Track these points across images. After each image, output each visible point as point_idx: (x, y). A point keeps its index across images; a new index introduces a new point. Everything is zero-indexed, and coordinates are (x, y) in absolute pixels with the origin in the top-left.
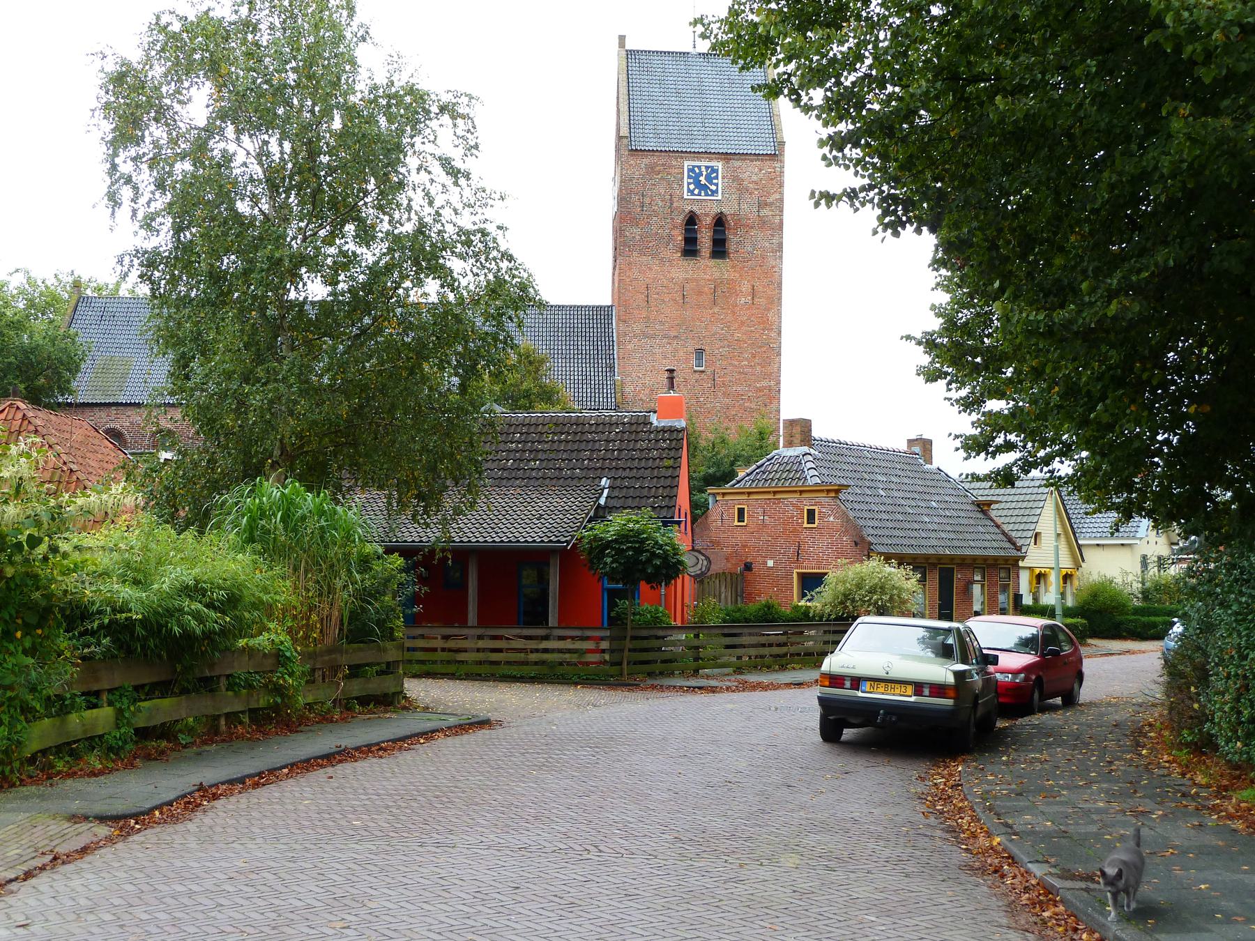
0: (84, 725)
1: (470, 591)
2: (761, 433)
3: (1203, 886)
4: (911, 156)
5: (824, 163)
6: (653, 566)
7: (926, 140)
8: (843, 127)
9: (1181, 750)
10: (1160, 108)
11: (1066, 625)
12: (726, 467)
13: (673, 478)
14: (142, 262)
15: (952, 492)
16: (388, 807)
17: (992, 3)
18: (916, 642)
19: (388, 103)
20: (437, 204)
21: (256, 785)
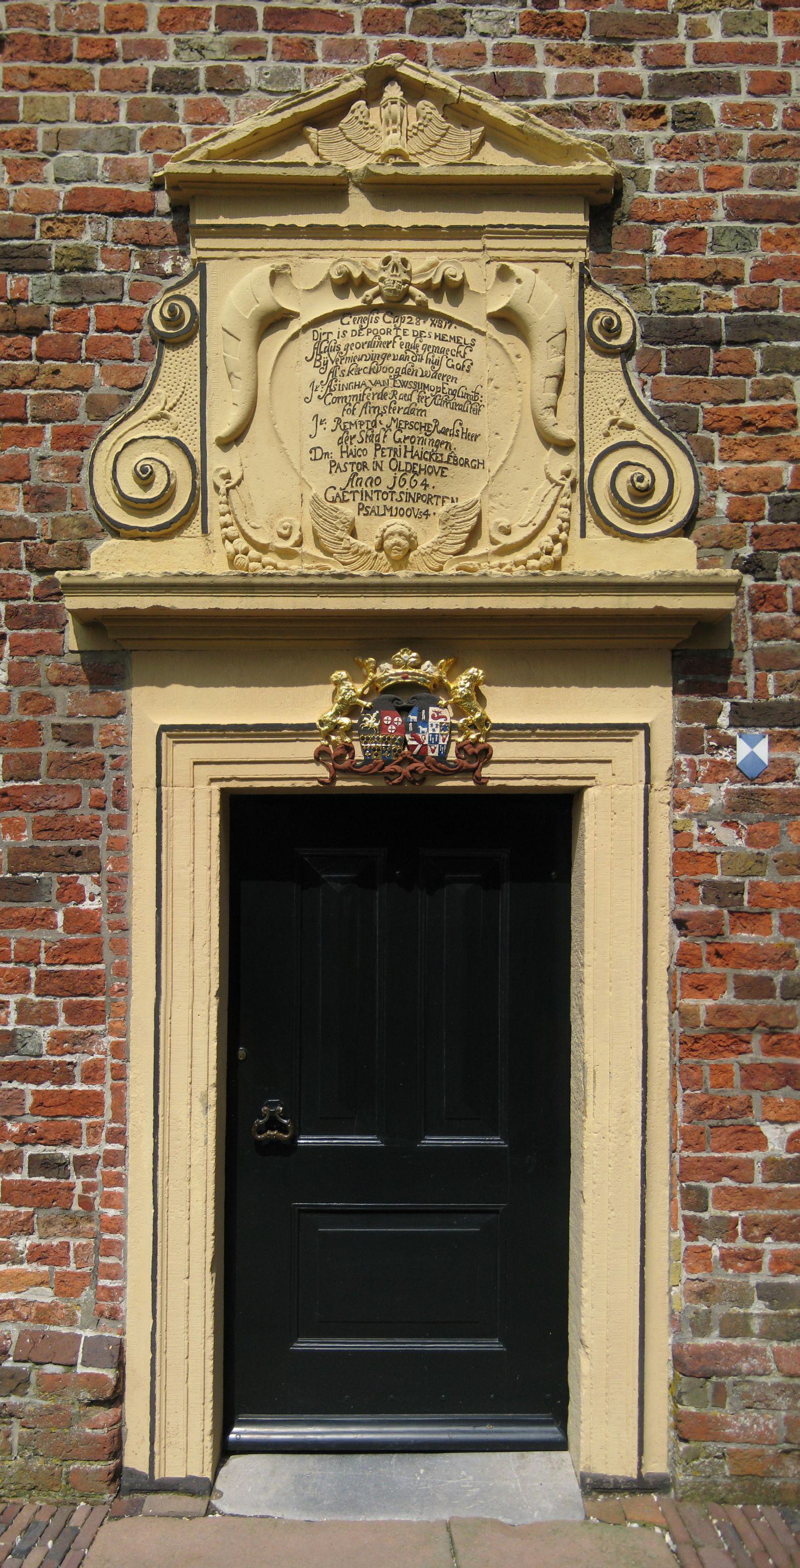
0: (669, 803)
1: (200, 606)
2: (477, 436)
3: (719, 1533)
4: (685, 1365)
5: (356, 274)
6: (711, 1382)
7: (755, 1426)
8: (445, 416)
9: (460, 749)
10: (421, 99)
11: (652, 406)
12: (140, 382)
13: (702, 1295)
14: (744, 1486)
15: (769, 548)
16: (43, 920)
17: (2, 1127)
18: (485, 318)
19: (382, 721)
20: (171, 414)
21: (671, 1217)
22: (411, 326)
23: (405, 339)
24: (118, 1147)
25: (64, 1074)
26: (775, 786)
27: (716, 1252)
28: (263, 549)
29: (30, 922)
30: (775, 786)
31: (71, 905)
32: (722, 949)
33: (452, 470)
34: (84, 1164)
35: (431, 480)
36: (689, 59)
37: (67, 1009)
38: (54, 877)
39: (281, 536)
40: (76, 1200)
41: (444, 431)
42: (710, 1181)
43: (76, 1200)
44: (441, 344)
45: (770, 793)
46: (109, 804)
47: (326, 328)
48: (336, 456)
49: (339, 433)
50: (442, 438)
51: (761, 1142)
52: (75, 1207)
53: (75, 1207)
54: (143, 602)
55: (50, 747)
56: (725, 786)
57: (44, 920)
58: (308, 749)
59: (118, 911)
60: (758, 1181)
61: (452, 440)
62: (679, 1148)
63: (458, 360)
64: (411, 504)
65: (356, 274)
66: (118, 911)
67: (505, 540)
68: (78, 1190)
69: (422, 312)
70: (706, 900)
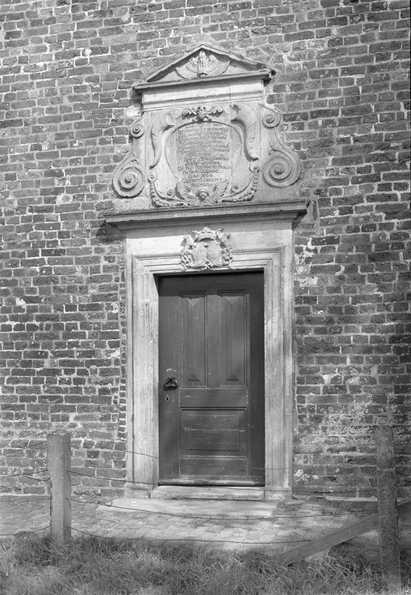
5: (190, 113)
22: (205, 126)
23: (205, 132)
24: (124, 385)
25: (109, 362)
26: (327, 264)
27: (53, 310)
28: (164, 199)
29: (98, 317)
30: (327, 264)
31: (109, 311)
32: (310, 319)
33: (221, 170)
34: (114, 390)
35: (214, 174)
36: (297, 28)
37: (110, 343)
38: (105, 303)
39: (168, 194)
40: (112, 402)
41: (217, 159)
42: (306, 394)
43: (112, 402)
44: (217, 131)
45: (325, 267)
46: (120, 280)
47: (181, 129)
48: (185, 169)
49: (186, 162)
50: (216, 161)
51: (319, 379)
52: (112, 403)
53: (112, 403)
54: (127, 219)
55: (104, 263)
56: (310, 265)
57: (102, 316)
58: (177, 260)
59: (123, 312)
60: (79, 323)
61: (220, 161)
62: (296, 383)
63: (222, 136)
64: (207, 182)
65: (190, 113)
66: (123, 312)
67: (237, 191)
68: (113, 398)
69: (210, 121)
70: (305, 303)
